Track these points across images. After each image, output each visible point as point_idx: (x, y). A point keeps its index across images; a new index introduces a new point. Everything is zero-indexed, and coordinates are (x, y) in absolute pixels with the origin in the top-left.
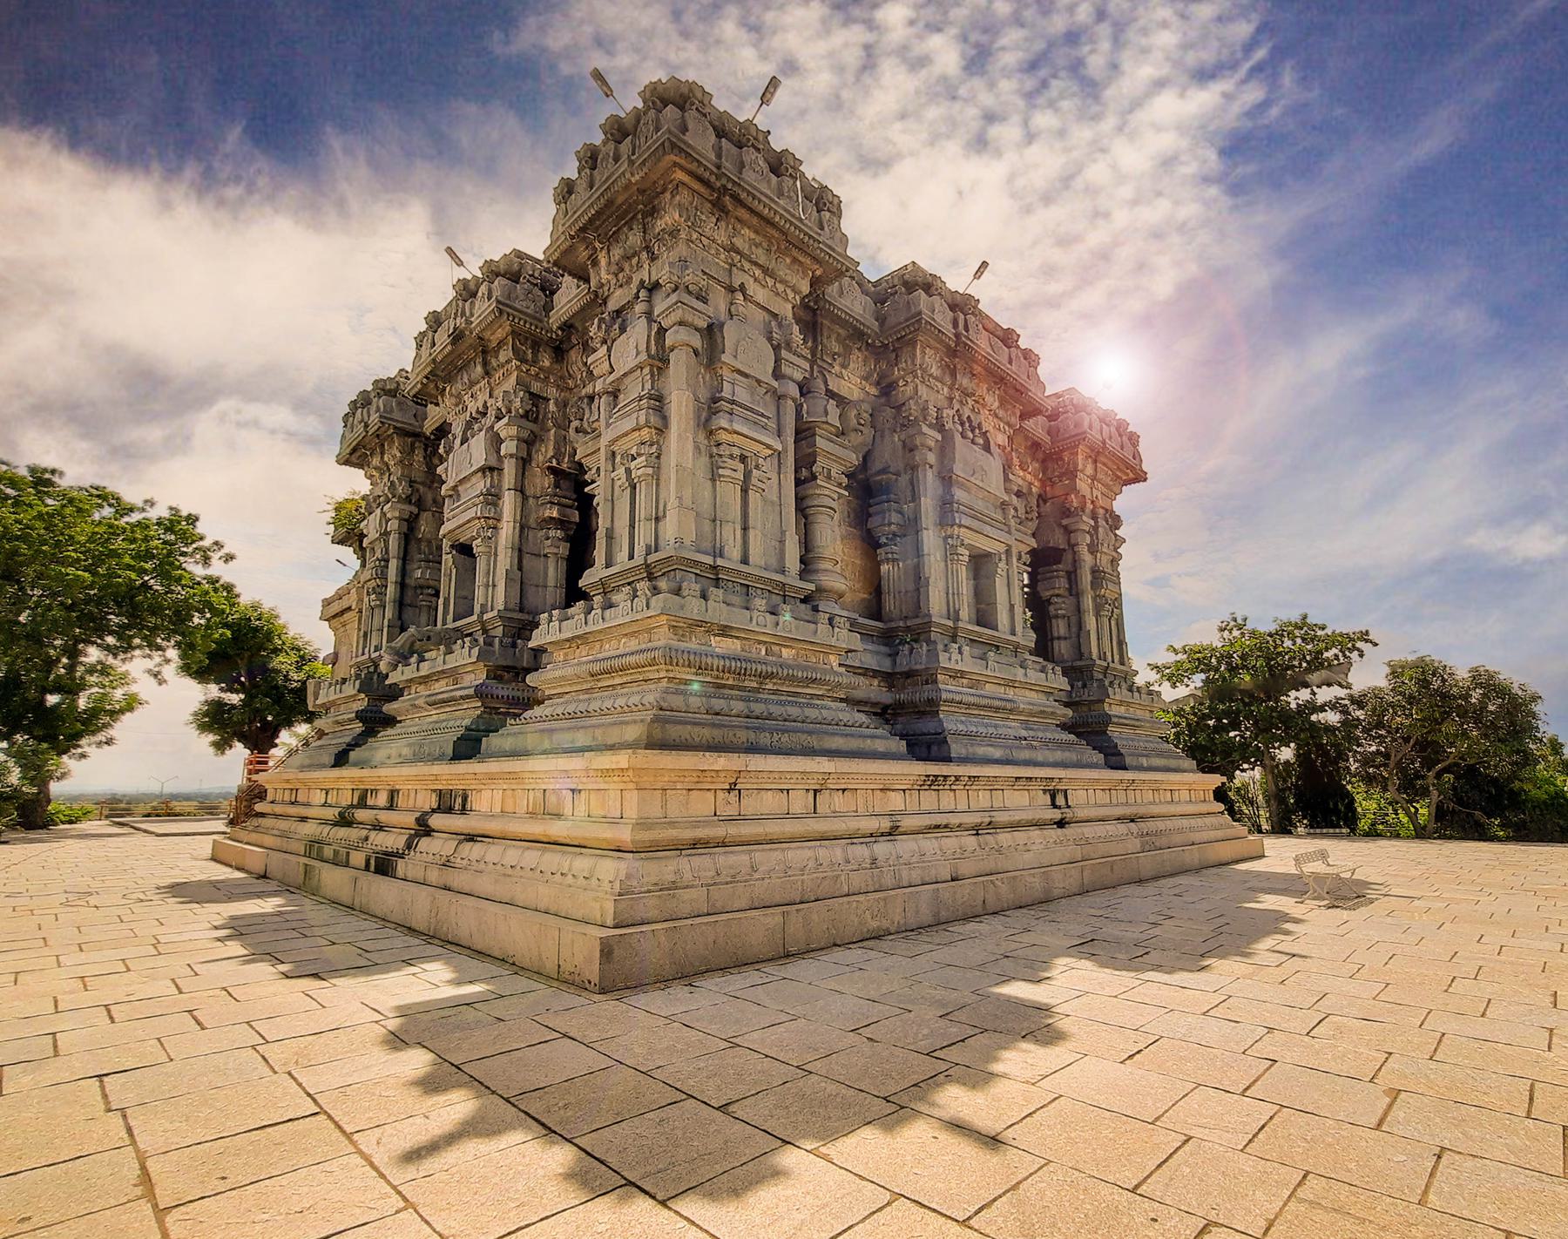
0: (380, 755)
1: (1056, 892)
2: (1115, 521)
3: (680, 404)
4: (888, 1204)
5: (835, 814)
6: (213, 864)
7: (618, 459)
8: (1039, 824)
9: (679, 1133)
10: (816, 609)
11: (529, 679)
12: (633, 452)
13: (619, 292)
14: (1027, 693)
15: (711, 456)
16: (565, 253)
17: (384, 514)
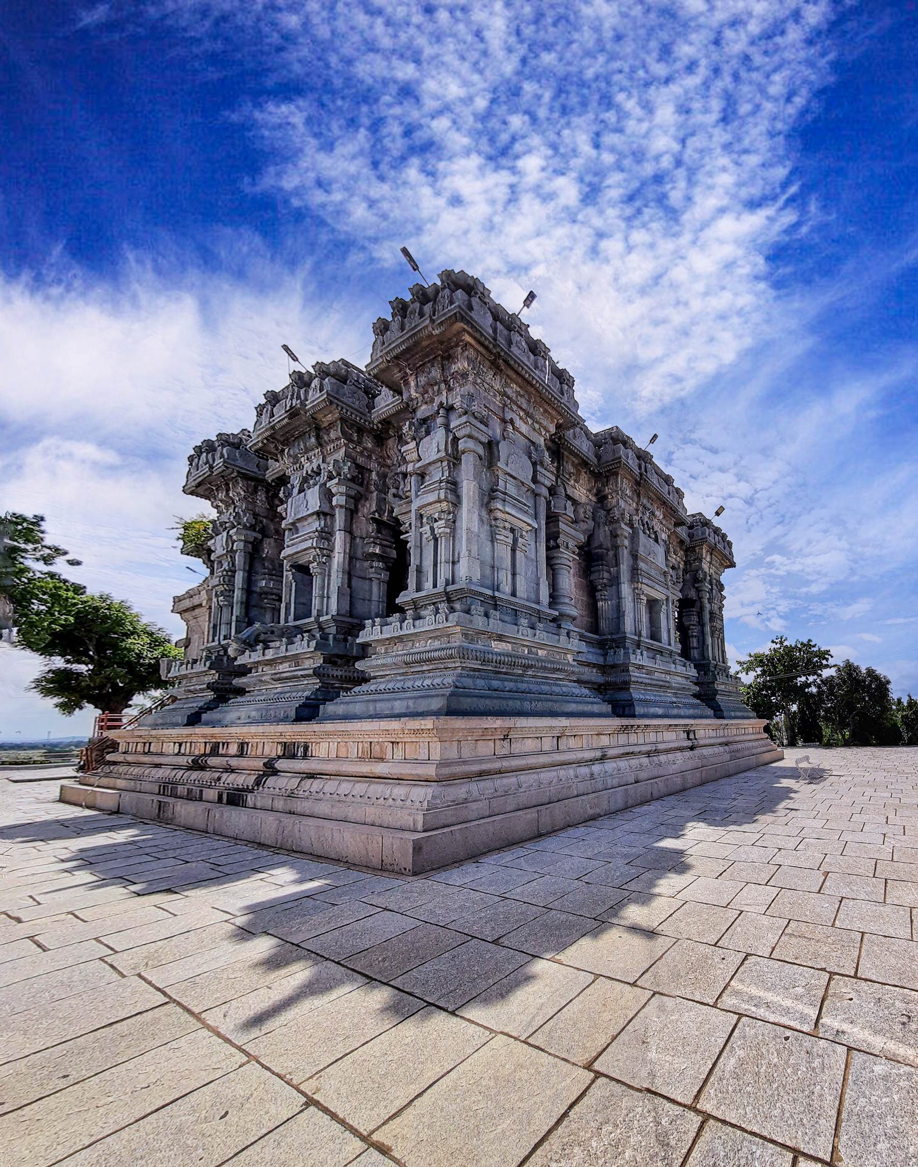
0: (232, 716)
1: (688, 785)
2: (721, 587)
3: (469, 489)
4: (593, 982)
5: (570, 750)
6: (62, 805)
7: (425, 520)
8: (681, 749)
9: (465, 963)
10: (559, 627)
11: (357, 665)
12: (436, 516)
13: (424, 407)
14: (676, 678)
15: (491, 526)
16: (383, 371)
17: (229, 536)
